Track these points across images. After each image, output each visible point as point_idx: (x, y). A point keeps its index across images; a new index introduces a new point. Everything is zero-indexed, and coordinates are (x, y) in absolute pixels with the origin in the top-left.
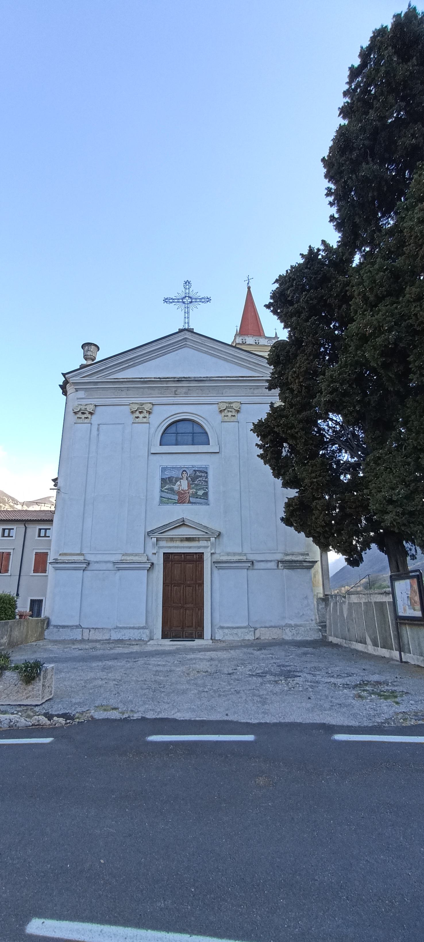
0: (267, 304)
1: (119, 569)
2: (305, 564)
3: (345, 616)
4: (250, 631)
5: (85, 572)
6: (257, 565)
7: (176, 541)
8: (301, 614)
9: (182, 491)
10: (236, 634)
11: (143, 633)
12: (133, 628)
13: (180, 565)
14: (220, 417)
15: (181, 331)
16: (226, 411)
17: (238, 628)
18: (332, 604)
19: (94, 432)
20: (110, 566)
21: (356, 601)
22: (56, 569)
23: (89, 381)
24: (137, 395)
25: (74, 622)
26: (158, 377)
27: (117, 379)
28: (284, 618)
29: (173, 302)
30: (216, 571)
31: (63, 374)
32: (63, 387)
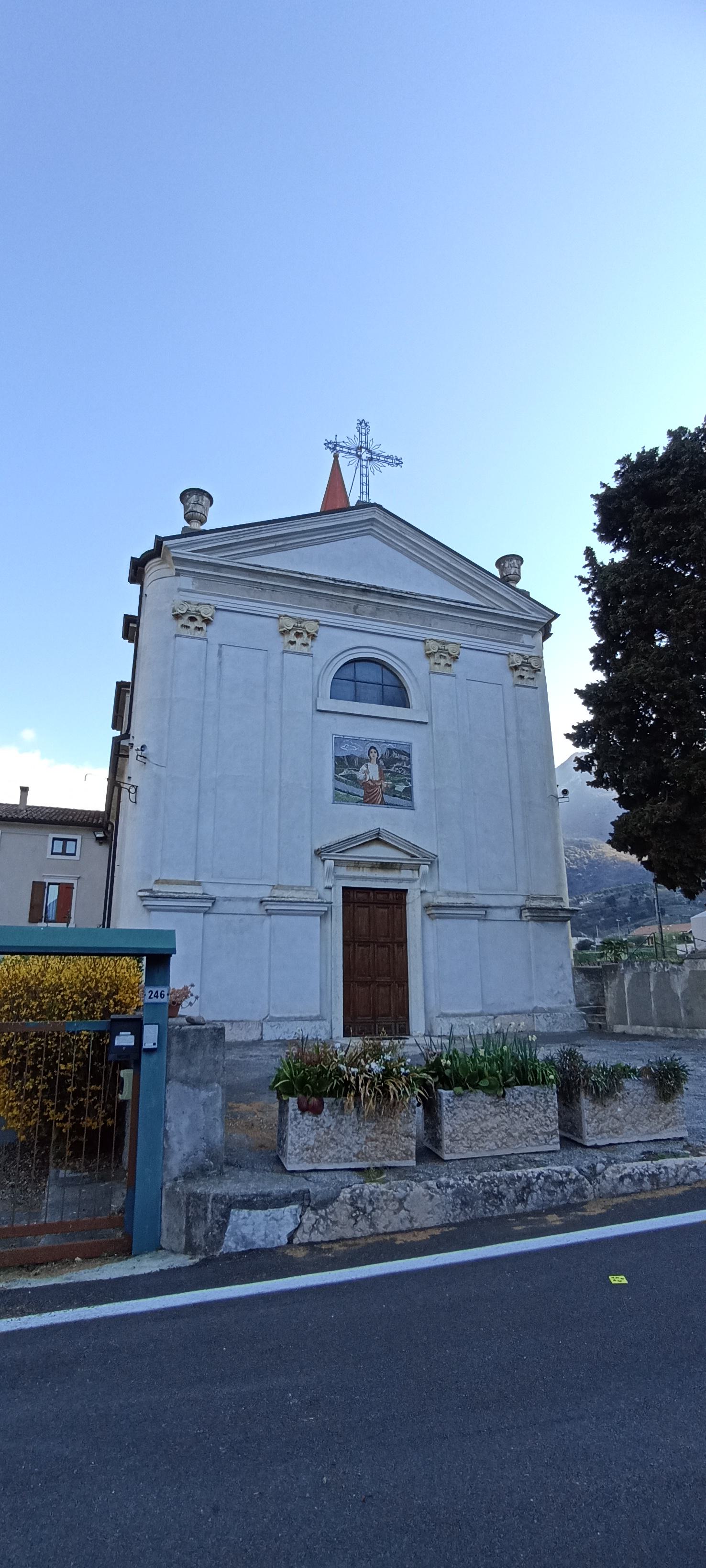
2: (561, 914)
4: (489, 1020)
5: (207, 916)
6: (221, 907)
8: (555, 992)
11: (321, 1028)
12: (301, 1019)
13: (367, 909)
14: (426, 664)
16: (437, 655)
17: (468, 1015)
19: (213, 659)
20: (254, 907)
23: (207, 560)
24: (291, 602)
26: (331, 577)
27: (260, 566)
28: (530, 999)
29: (386, 457)
30: (428, 922)
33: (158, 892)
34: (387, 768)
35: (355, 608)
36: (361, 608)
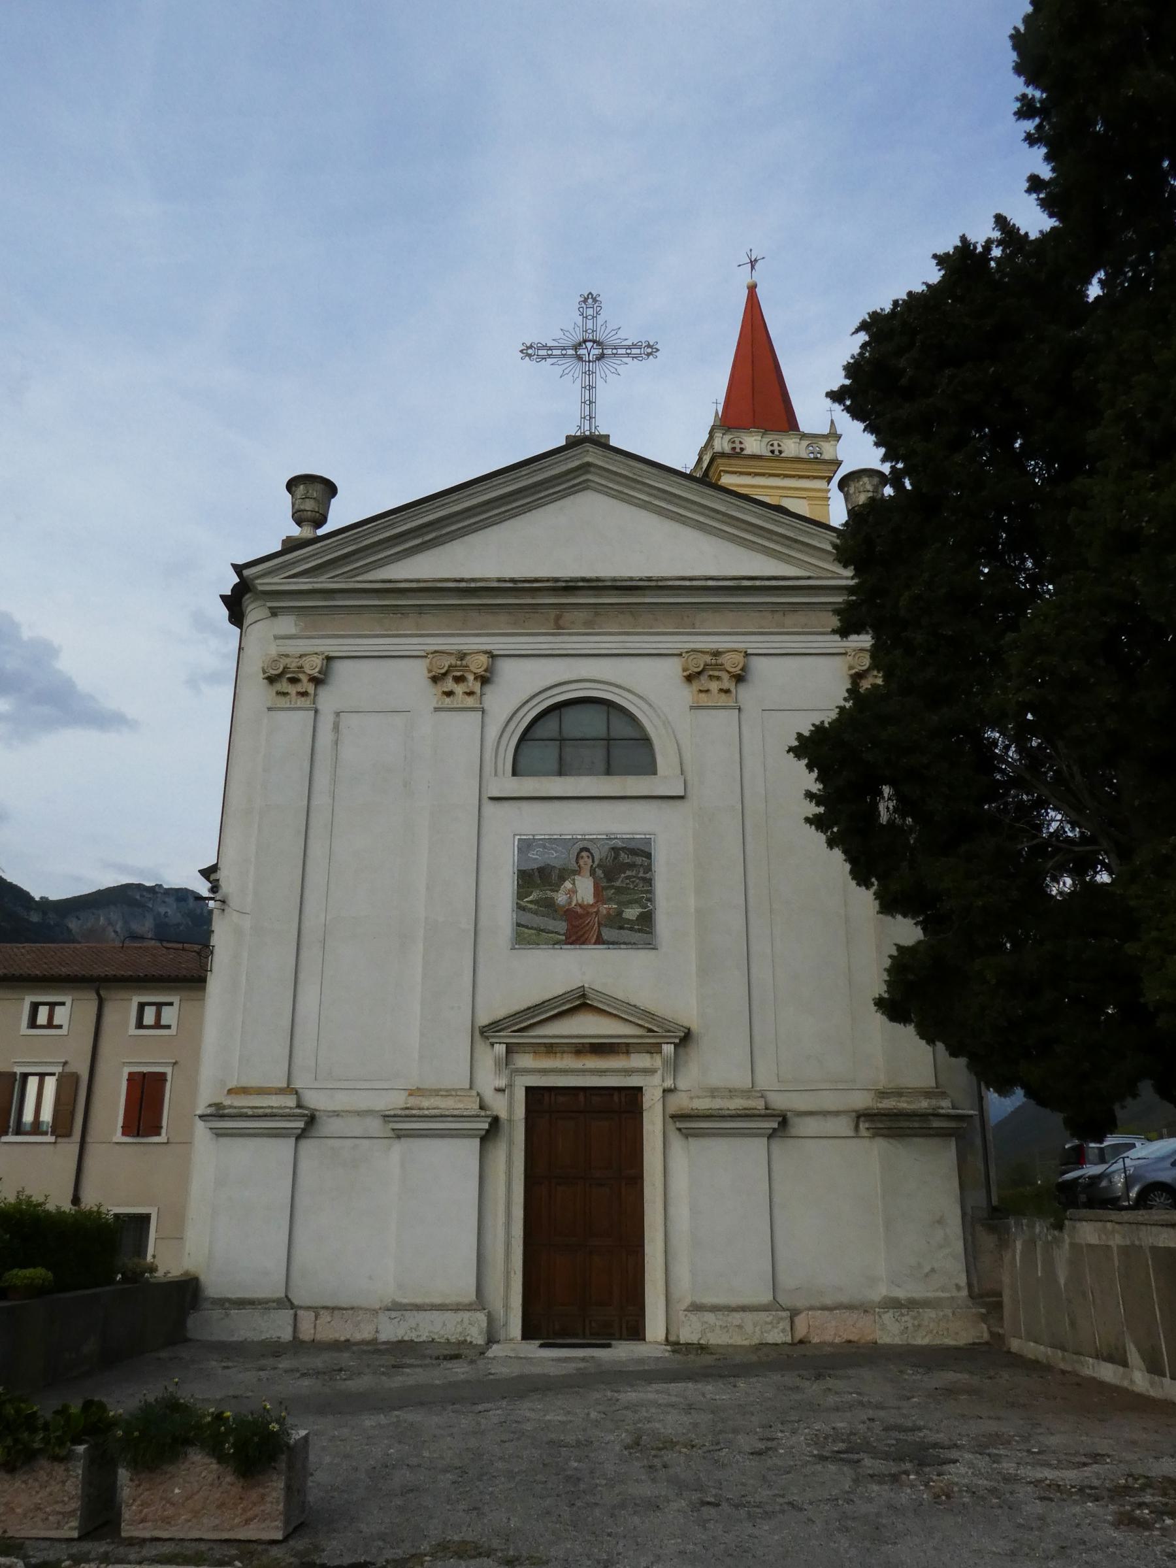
0: (835, 389)
1: (399, 1135)
2: (936, 1124)
3: (1062, 1281)
5: (305, 1144)
7: (563, 1052)
8: (927, 1269)
9: (579, 910)
10: (740, 1327)
15: (574, 443)
18: (1019, 1245)
20: (375, 1126)
21: (1093, 1239)
22: (219, 1134)
25: (272, 1288)
27: (390, 581)
29: (550, 356)
30: (677, 1144)
31: (235, 566)
32: (235, 605)
33: (231, 1107)
34: (610, 880)
35: (558, 618)
36: (568, 616)
